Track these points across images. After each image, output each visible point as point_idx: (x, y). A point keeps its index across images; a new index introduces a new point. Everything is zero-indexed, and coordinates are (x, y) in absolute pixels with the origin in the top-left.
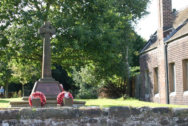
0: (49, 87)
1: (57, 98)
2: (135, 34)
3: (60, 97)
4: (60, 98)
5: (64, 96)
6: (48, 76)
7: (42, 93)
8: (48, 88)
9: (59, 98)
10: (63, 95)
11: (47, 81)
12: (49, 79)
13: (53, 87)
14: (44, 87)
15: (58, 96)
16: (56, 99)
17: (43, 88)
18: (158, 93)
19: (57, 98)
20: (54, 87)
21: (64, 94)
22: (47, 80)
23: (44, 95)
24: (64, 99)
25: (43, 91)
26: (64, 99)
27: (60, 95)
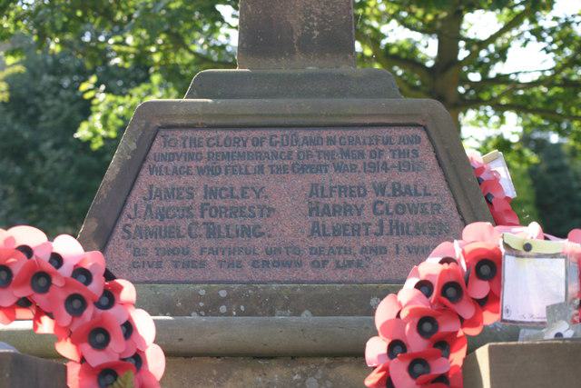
0: (302, 182)
1: (376, 349)
2: (376, 305)
3: (424, 322)
4: (417, 344)
5: (492, 300)
6: (306, 46)
7: (93, 260)
8: (286, 198)
9: (396, 347)
10: (480, 289)
11: (286, 105)
12: (311, 77)
13: (368, 179)
14: (237, 181)
15: (384, 312)
16: (360, 354)
17: (211, 192)
18: (85, 251)
19: (376, 349)
20: (382, 178)
21: (488, 266)
22: (289, 85)
23: (128, 292)
24: (482, 354)
25: (212, 232)
26: (482, 354)
27: (424, 286)
